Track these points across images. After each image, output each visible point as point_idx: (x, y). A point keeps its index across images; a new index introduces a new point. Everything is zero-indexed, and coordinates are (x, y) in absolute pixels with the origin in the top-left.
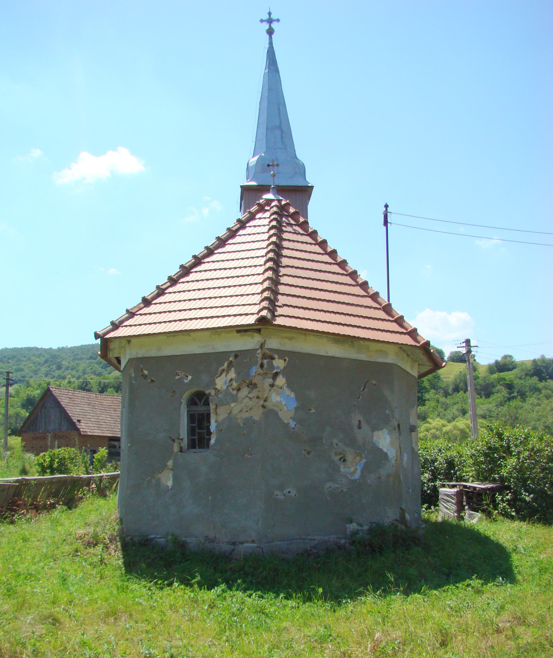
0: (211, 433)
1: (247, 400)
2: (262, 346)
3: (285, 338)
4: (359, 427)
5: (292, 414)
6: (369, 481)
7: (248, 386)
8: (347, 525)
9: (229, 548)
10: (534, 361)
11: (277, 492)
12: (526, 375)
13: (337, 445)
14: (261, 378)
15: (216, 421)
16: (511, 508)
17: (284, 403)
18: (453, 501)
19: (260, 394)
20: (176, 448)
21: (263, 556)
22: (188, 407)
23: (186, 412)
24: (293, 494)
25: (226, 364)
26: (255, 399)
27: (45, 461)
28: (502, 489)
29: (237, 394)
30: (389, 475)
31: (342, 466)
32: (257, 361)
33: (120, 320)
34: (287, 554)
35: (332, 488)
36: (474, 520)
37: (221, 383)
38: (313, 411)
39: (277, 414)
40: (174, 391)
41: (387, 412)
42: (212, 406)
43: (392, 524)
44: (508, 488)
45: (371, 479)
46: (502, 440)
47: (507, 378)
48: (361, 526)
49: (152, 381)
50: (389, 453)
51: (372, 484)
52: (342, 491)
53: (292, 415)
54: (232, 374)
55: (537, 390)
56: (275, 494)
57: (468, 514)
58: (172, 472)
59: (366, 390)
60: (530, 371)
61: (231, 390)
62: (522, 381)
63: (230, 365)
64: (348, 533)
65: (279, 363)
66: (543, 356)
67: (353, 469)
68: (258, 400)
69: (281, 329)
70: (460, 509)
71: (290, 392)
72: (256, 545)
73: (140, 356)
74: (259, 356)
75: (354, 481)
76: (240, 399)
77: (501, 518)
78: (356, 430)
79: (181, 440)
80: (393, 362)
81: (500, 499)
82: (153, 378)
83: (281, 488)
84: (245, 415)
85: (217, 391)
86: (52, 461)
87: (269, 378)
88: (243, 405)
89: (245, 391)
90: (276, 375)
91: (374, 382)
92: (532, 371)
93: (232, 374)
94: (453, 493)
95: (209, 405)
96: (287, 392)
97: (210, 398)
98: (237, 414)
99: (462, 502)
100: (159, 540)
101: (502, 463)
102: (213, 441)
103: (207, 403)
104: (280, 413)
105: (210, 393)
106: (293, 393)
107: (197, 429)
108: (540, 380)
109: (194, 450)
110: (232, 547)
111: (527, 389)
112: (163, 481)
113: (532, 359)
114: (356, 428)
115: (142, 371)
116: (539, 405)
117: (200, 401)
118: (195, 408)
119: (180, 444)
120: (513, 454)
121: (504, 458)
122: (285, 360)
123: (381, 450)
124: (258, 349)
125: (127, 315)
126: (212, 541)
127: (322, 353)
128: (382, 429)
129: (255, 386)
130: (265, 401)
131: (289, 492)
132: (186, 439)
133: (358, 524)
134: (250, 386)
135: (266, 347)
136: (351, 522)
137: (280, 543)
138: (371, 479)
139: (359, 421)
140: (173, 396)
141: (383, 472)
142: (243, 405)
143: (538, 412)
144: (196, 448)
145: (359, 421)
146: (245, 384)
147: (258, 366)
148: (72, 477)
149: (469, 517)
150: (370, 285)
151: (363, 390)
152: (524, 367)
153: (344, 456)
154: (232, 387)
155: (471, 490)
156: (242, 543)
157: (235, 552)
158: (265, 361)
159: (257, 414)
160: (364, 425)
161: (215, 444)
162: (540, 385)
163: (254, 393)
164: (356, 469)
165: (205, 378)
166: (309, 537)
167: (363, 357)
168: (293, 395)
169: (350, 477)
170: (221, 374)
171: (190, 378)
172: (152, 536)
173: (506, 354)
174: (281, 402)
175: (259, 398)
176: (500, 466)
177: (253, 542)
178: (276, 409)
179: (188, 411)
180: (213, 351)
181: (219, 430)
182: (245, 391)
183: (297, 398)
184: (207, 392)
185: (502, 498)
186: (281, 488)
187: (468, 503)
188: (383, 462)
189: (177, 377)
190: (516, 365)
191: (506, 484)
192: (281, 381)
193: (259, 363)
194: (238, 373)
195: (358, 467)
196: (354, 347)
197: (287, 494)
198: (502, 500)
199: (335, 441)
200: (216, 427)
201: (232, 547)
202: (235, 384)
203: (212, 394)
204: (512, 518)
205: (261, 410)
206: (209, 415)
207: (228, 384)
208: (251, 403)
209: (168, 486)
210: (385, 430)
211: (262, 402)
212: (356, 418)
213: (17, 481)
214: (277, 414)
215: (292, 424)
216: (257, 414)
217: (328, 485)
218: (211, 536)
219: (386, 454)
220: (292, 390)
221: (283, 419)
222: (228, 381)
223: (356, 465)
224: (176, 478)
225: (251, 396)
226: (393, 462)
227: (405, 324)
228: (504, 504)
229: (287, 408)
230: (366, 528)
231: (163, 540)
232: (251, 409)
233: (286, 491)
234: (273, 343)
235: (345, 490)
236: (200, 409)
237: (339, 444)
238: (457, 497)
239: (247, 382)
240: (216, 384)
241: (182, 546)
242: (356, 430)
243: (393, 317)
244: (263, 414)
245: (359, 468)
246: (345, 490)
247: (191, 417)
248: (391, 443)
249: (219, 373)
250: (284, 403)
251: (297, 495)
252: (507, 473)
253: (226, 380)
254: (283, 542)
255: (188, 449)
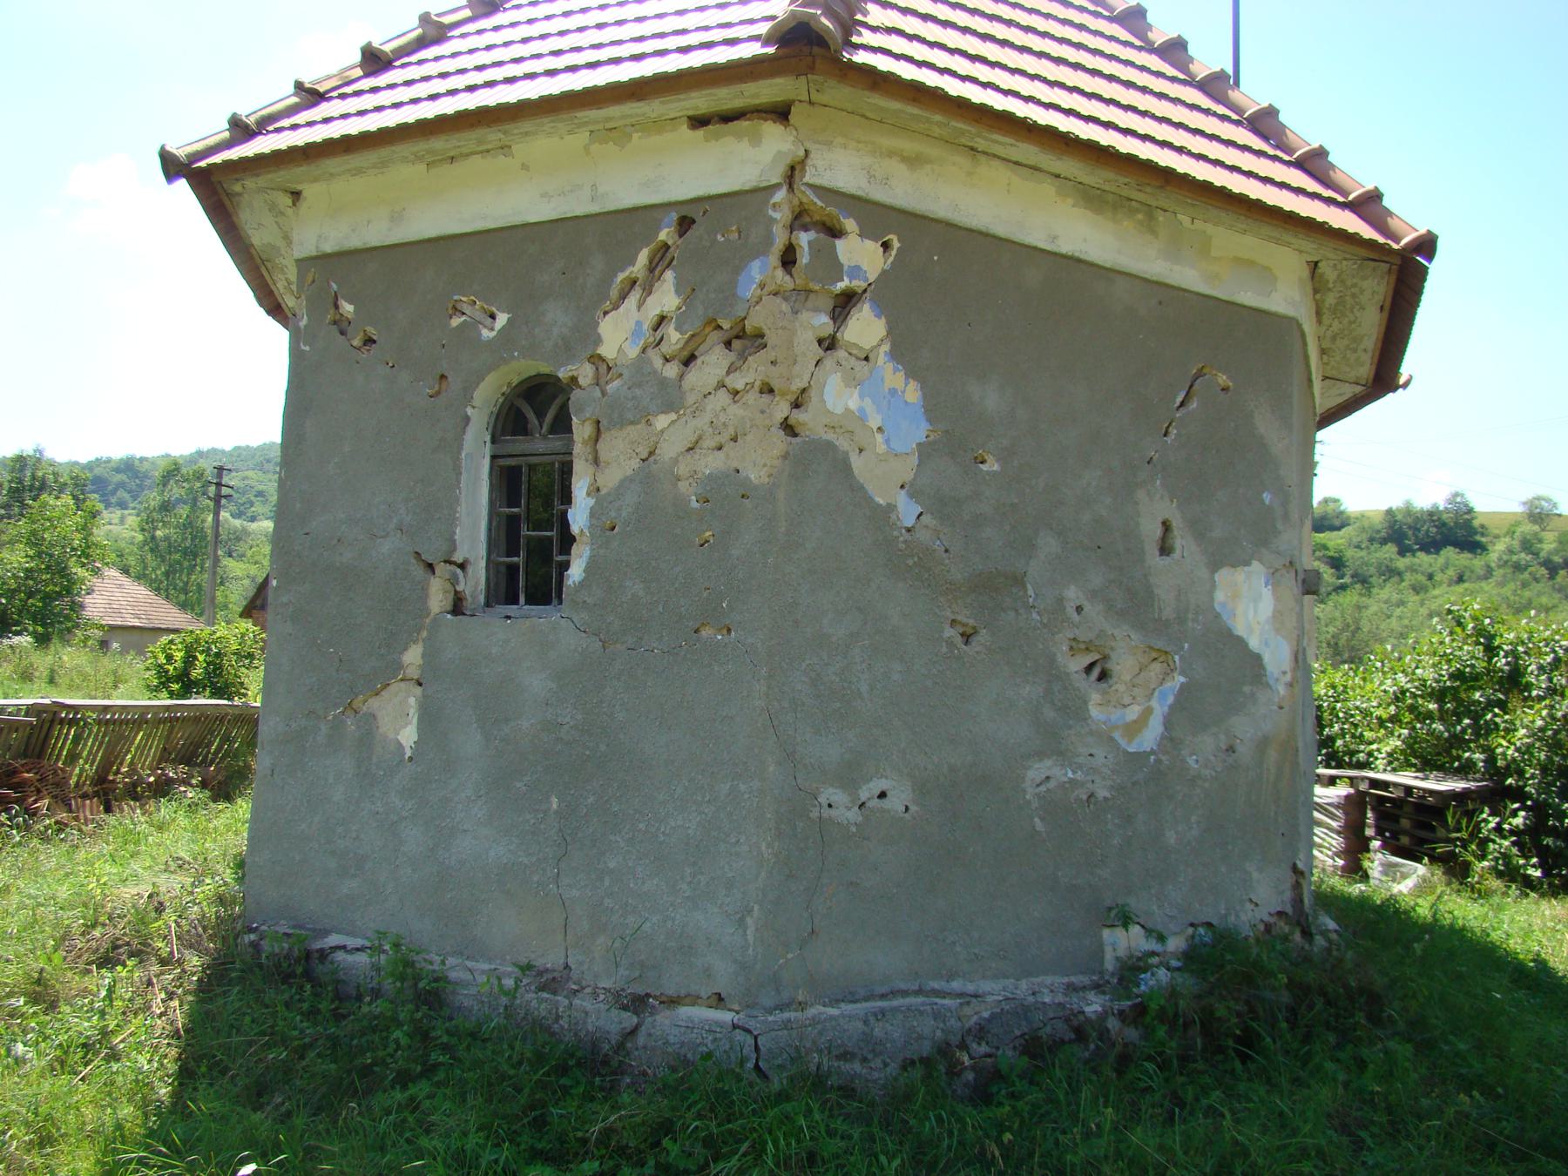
0: (573, 539)
1: (723, 397)
2: (792, 173)
3: (891, 154)
4: (1165, 550)
5: (906, 469)
6: (1191, 761)
7: (728, 344)
8: (1106, 933)
9: (614, 1022)
10: (1389, 512)
11: (830, 794)
12: (1371, 540)
13: (1079, 609)
14: (785, 307)
15: (595, 490)
16: (1527, 858)
17: (874, 421)
18: (1334, 824)
19: (775, 378)
20: (438, 598)
21: (757, 1066)
22: (493, 441)
23: (487, 462)
24: (895, 803)
25: (643, 257)
26: (752, 398)
27: (169, 658)
28: (1498, 795)
29: (681, 377)
30: (1263, 744)
31: (1095, 697)
32: (768, 240)
33: (264, 113)
34: (865, 1060)
35: (1052, 784)
36: (1404, 882)
37: (618, 334)
38: (992, 466)
39: (843, 467)
40: (443, 377)
41: (1267, 497)
42: (581, 430)
43: (1268, 928)
44: (1518, 794)
45: (1201, 753)
46: (1491, 651)
47: (1331, 544)
48: (1161, 938)
49: (369, 341)
50: (1267, 658)
51: (1207, 772)
52: (1091, 795)
53: (908, 476)
54: (666, 298)
55: (1391, 573)
56: (823, 800)
57: (1382, 865)
58: (419, 690)
59: (1193, 405)
60: (1378, 532)
61: (658, 362)
62: (1363, 553)
63: (661, 258)
64: (1109, 964)
65: (861, 256)
66: (1408, 504)
67: (1136, 710)
68: (766, 398)
69: (878, 100)
70: (1355, 849)
71: (901, 375)
72: (726, 1017)
73: (328, 248)
74: (777, 215)
75: (1140, 757)
76: (690, 399)
77: (1495, 883)
78: (1154, 559)
79: (462, 566)
80: (1291, 313)
81: (1492, 825)
82: (371, 330)
83: (849, 777)
84: (710, 463)
85: (603, 368)
86: (190, 660)
87: (816, 310)
88: (702, 422)
89: (714, 362)
90: (845, 304)
91: (1222, 379)
92: (1383, 534)
93: (666, 298)
94: (1335, 800)
95: (568, 429)
96: (891, 376)
97: (576, 395)
98: (676, 461)
99: (1363, 825)
100: (350, 958)
101: (1497, 720)
102: (576, 572)
103: (562, 425)
104: (856, 462)
105: (574, 380)
106: (913, 386)
107: (524, 527)
108: (1402, 553)
109: (511, 609)
110: (629, 1019)
111: (1372, 570)
112: (385, 725)
113: (1385, 508)
114: (1152, 550)
115: (337, 307)
116: (1401, 603)
117: (540, 415)
118: (519, 445)
119: (453, 581)
120: (1534, 693)
121: (1502, 705)
122: (886, 246)
123: (1241, 643)
124: (777, 187)
125: (295, 100)
126: (551, 982)
127: (1037, 239)
128: (1247, 563)
129: (756, 340)
130: (797, 405)
131: (882, 795)
132: (483, 564)
133: (1149, 931)
134: (736, 344)
135: (807, 179)
136: (1126, 920)
137: (834, 1011)
138: (1201, 753)
139: (1166, 526)
140: (438, 393)
141: (1244, 729)
142: (702, 422)
143: (1400, 618)
144: (516, 602)
145: (1166, 526)
146: (715, 336)
147: (774, 259)
148: (247, 706)
149: (1385, 873)
150: (1192, 50)
151: (1182, 404)
152: (1366, 524)
153: (1105, 658)
154: (664, 348)
155: (1400, 794)
156: (673, 1002)
157: (641, 1039)
158: (804, 239)
159: (760, 460)
160: (1182, 541)
161: (582, 584)
162: (1402, 563)
163: (755, 370)
164: (1148, 712)
165: (557, 318)
166: (956, 985)
167: (1187, 276)
168: (913, 393)
169: (1123, 742)
170: (623, 297)
171: (502, 319)
172: (334, 940)
173: (1327, 495)
174: (862, 418)
175: (771, 391)
176: (1492, 728)
177: (719, 1000)
178: (843, 444)
179: (494, 457)
180: (594, 208)
181: (604, 527)
182: (714, 362)
183: (932, 410)
184: (563, 374)
185: (1499, 825)
186: (849, 777)
187: (1380, 832)
188: (1247, 689)
189: (456, 321)
190: (1349, 518)
191: (1509, 781)
192: (865, 327)
193: (780, 240)
194: (689, 292)
195: (1154, 703)
196: (1154, 232)
197: (875, 803)
198: (1498, 829)
199: (1073, 594)
200: (593, 514)
201: (629, 1019)
202: (674, 337)
203: (581, 381)
204: (1528, 884)
205: (779, 440)
206: (566, 471)
207: (647, 335)
208: (736, 411)
209: (400, 746)
210: (1256, 565)
211: (781, 409)
212: (1154, 509)
213: (31, 710)
214: (847, 468)
215: (907, 511)
216: (760, 460)
217: (1037, 771)
218: (551, 959)
219: (1257, 659)
220: (911, 374)
221: (870, 488)
222: (646, 326)
223: (1150, 696)
224: (429, 719)
225: (740, 386)
226: (1282, 690)
227: (1337, 177)
228: (1506, 843)
229: (887, 441)
230: (1175, 944)
231: (363, 958)
232: (735, 440)
233: (867, 791)
234: (841, 168)
235: (1102, 793)
236: (540, 445)
237: (1087, 607)
238: (1346, 813)
239: (726, 326)
240: (598, 340)
241: (431, 996)
242: (1154, 559)
243: (1289, 151)
244: (785, 457)
245: (1159, 709)
246: (1102, 793)
247: (509, 481)
248: (1277, 616)
249: (614, 293)
250: (874, 421)
251: (913, 808)
252: (1517, 750)
253: (638, 323)
254: (848, 1008)
255: (488, 604)
